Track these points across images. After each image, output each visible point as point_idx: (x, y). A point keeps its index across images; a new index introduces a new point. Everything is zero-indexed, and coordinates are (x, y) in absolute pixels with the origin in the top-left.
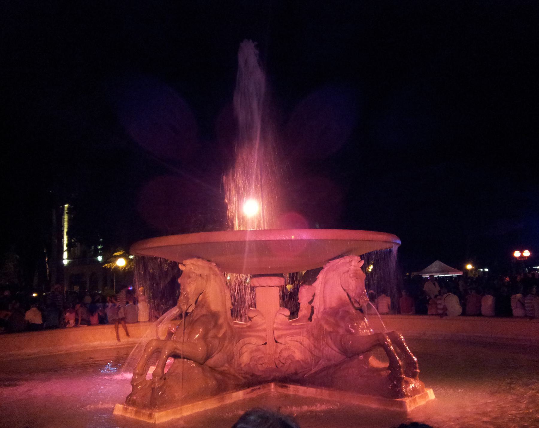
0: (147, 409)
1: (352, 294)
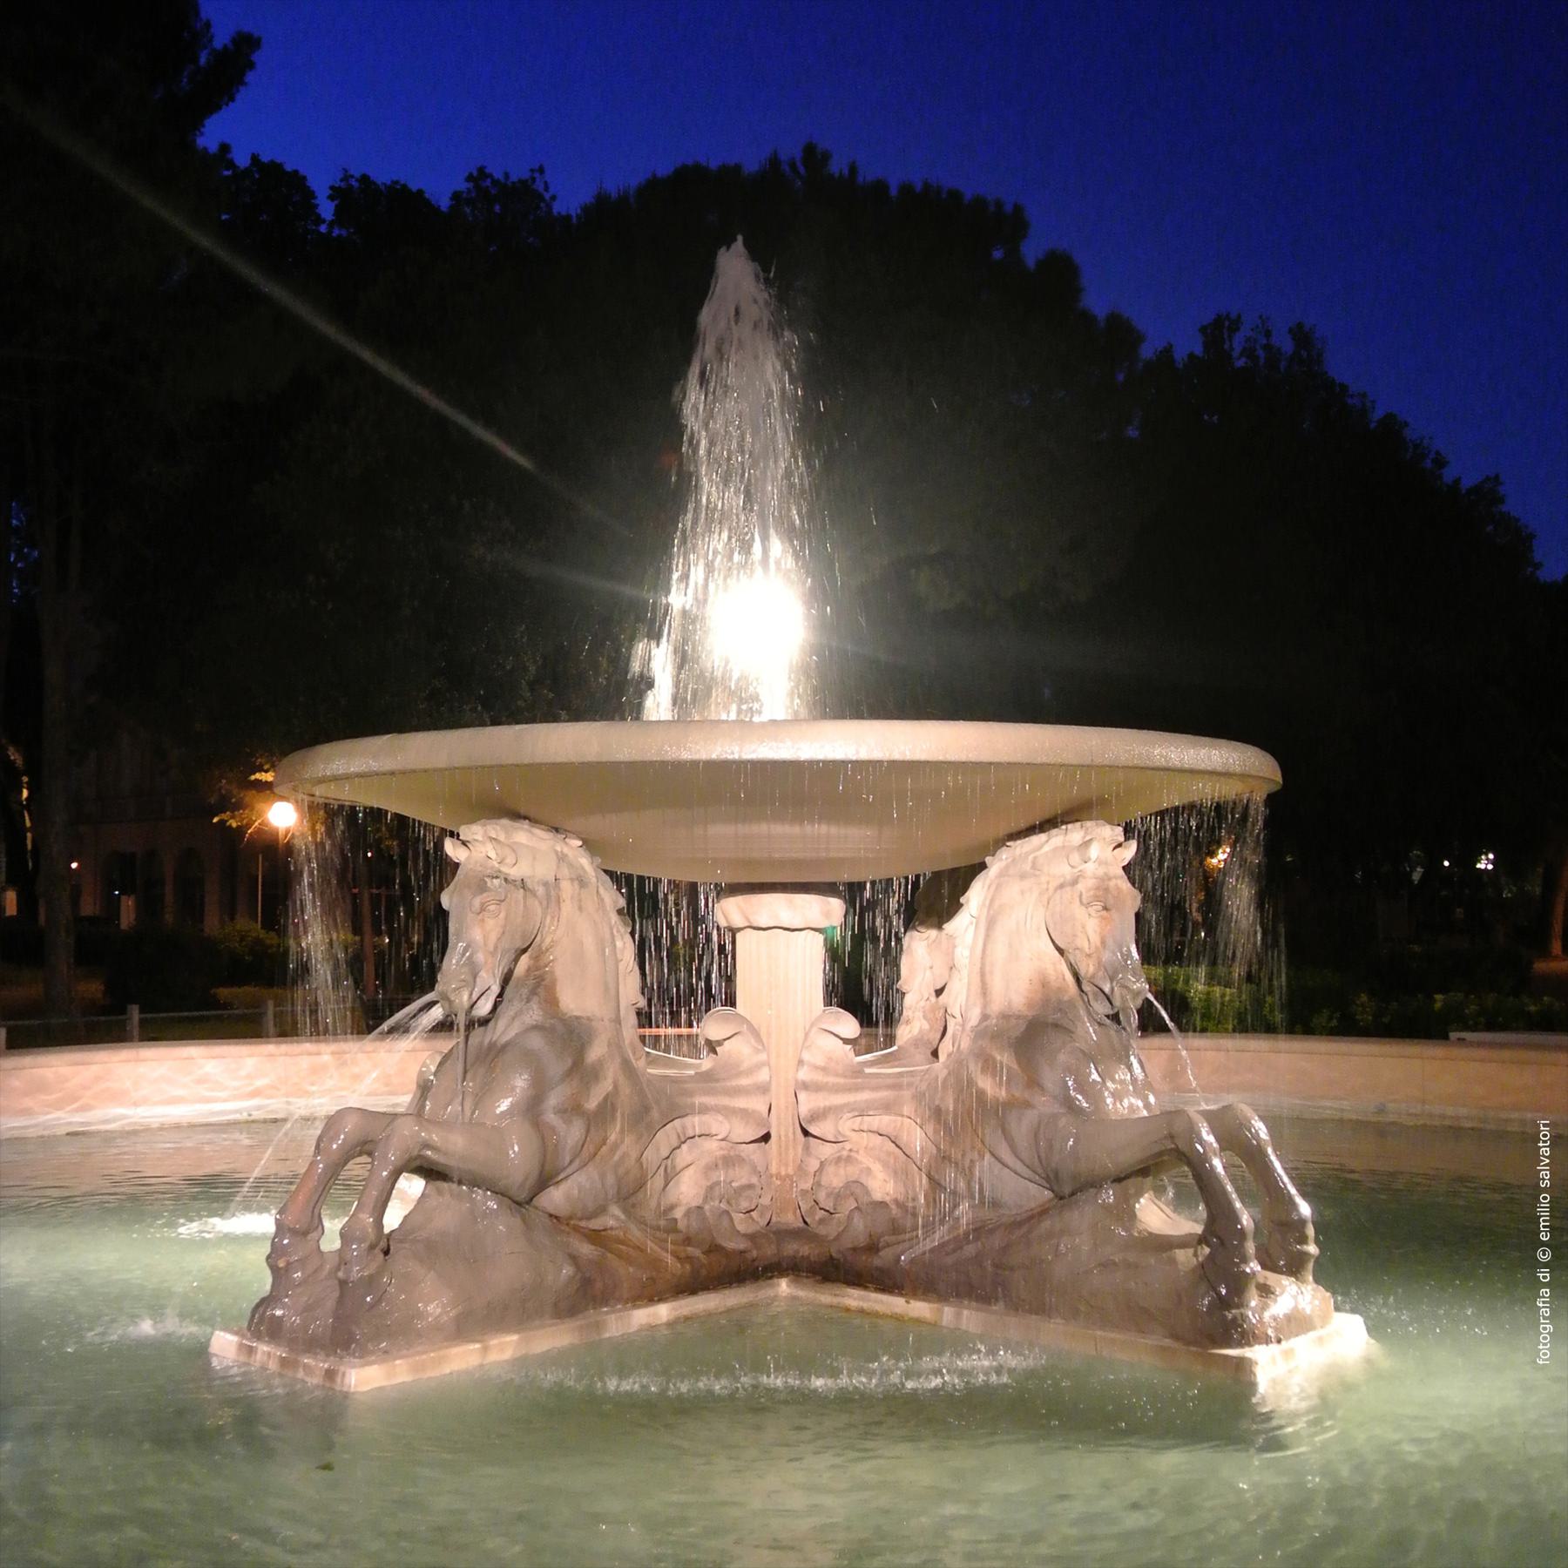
0: (322, 1356)
1: (1087, 968)
